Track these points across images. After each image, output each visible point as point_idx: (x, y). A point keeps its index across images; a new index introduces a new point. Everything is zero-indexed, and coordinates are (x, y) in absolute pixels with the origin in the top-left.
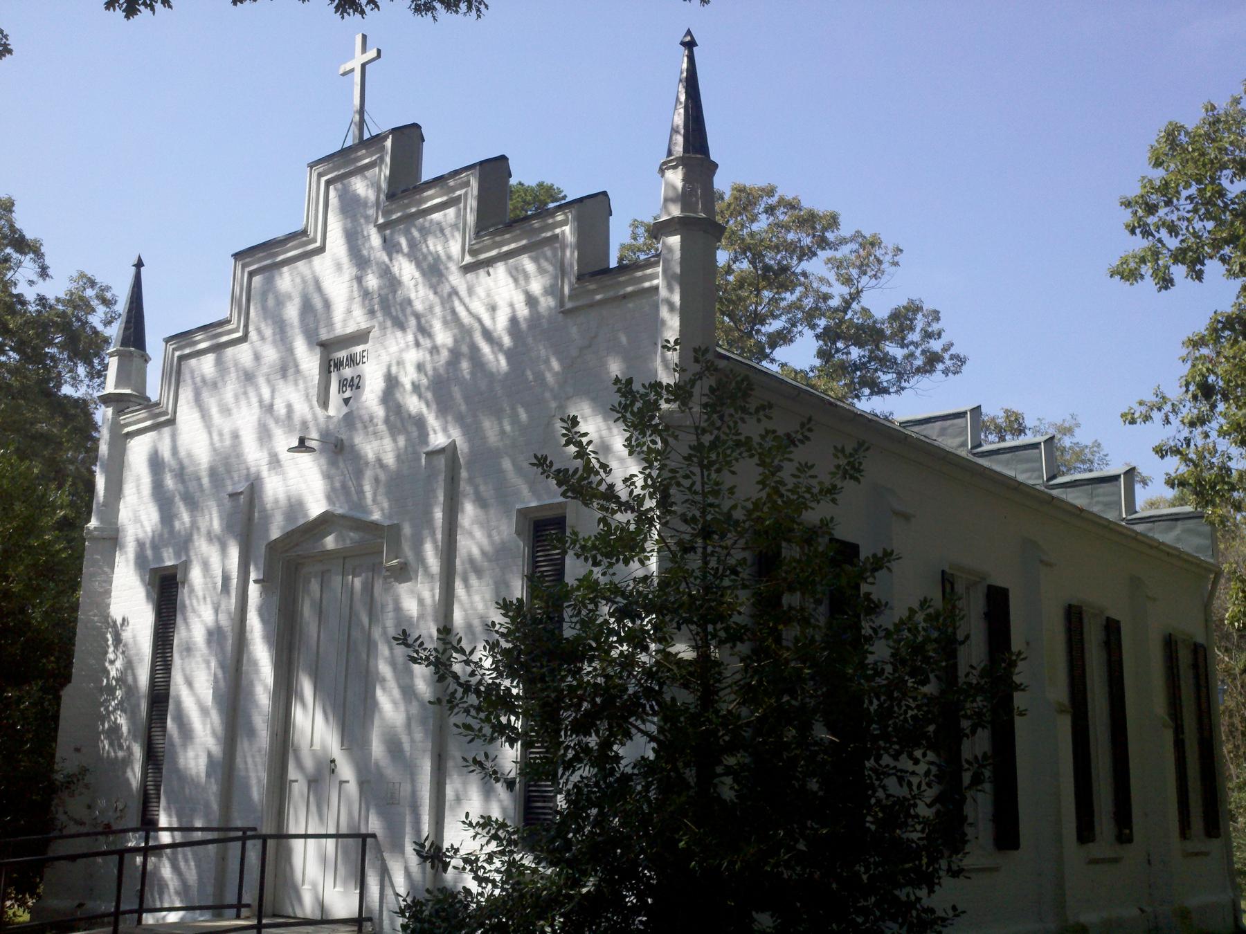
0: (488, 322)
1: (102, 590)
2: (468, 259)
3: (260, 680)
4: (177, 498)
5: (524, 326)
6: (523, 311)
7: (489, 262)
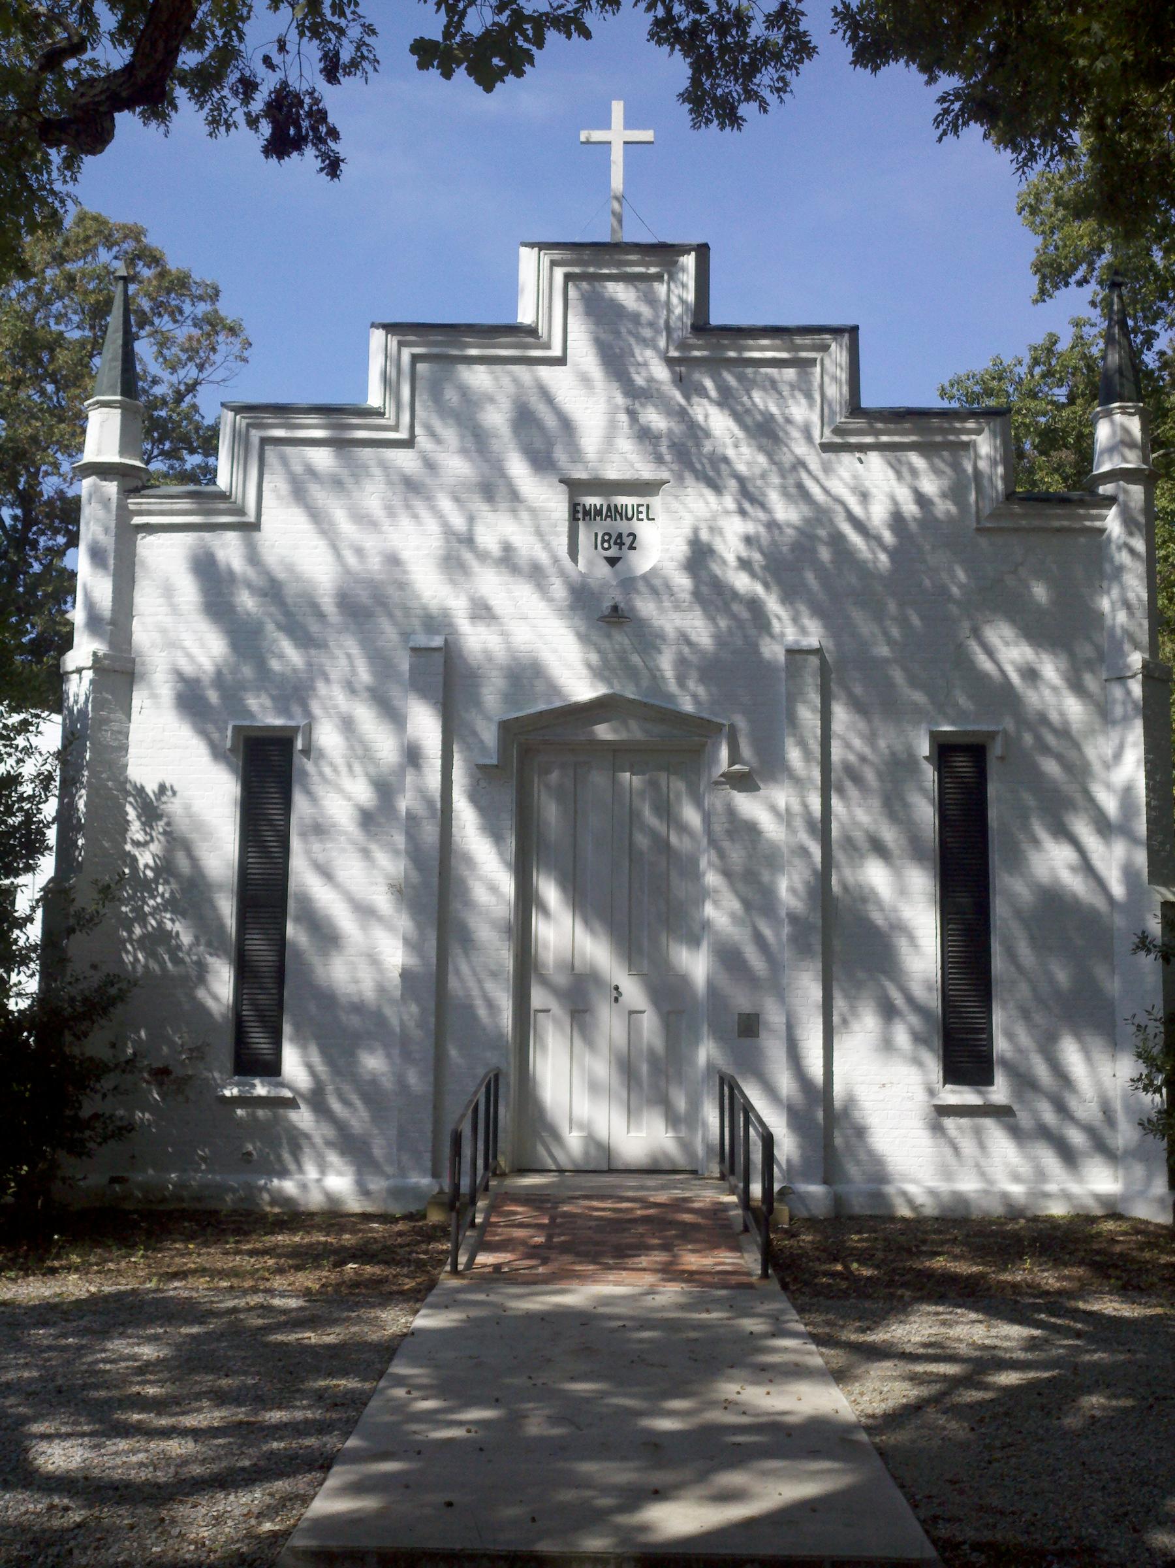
0: (857, 509)
1: (115, 744)
2: (829, 437)
3: (480, 878)
4: (270, 627)
5: (913, 527)
6: (910, 508)
7: (863, 448)
